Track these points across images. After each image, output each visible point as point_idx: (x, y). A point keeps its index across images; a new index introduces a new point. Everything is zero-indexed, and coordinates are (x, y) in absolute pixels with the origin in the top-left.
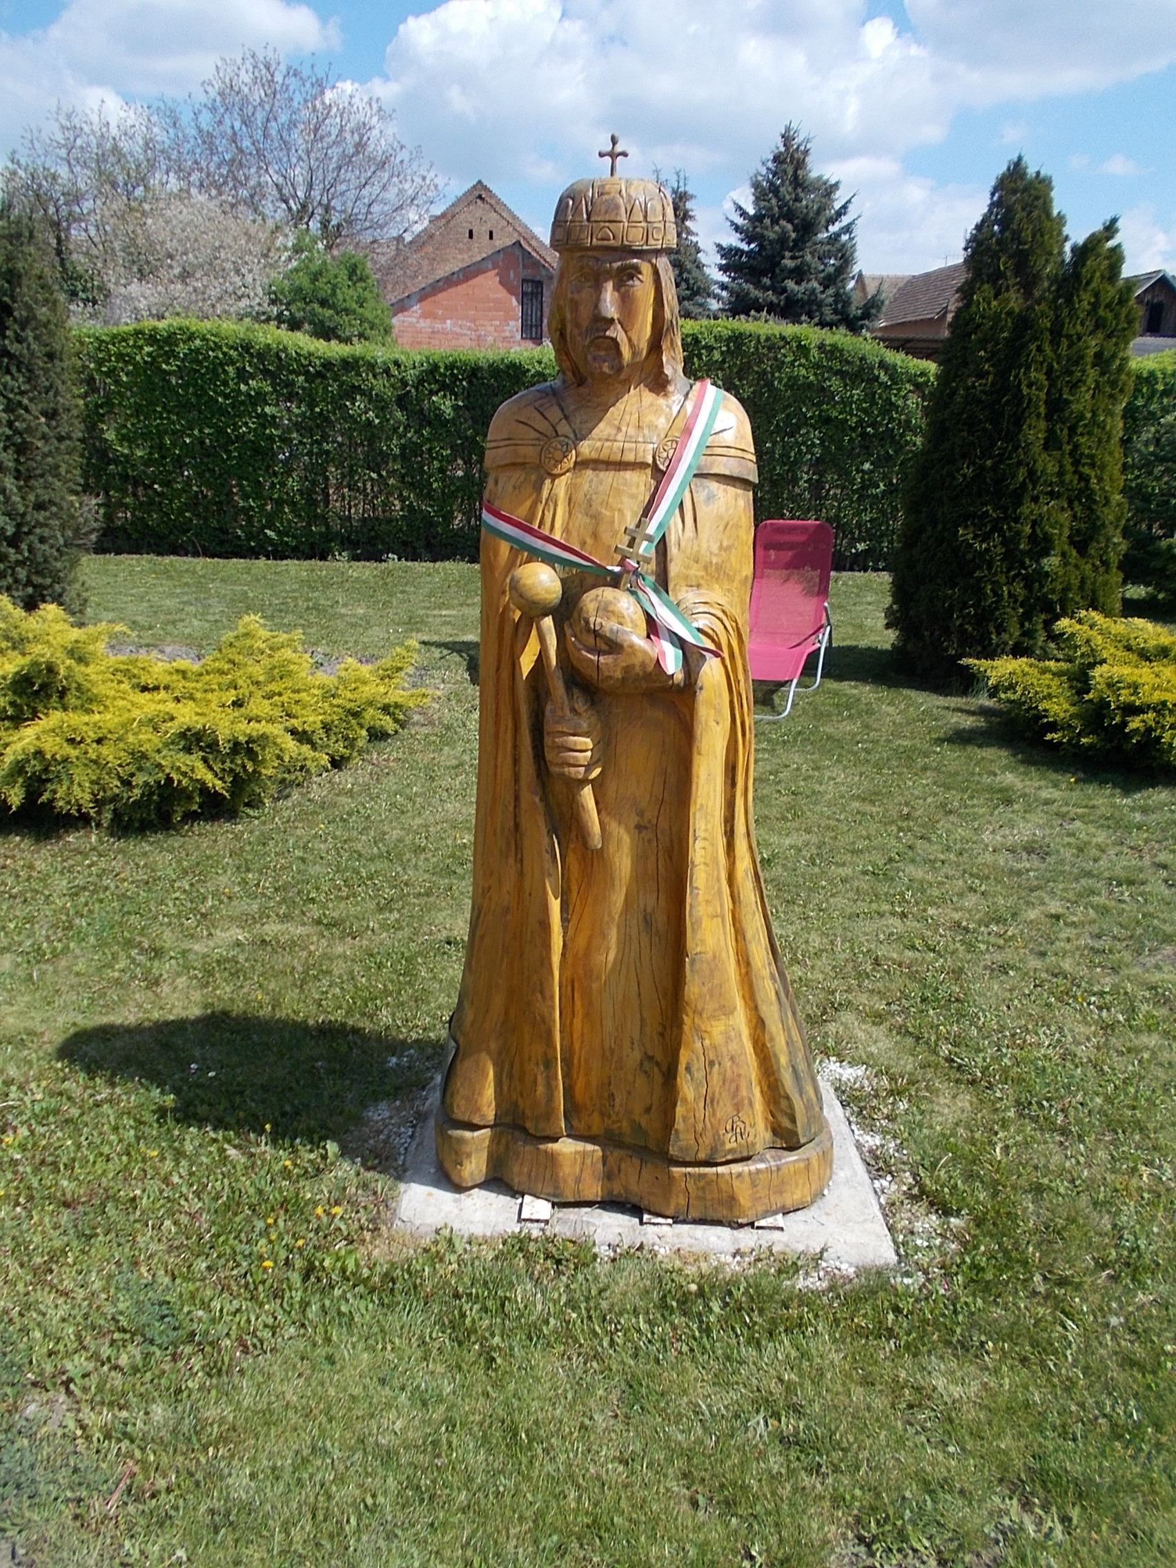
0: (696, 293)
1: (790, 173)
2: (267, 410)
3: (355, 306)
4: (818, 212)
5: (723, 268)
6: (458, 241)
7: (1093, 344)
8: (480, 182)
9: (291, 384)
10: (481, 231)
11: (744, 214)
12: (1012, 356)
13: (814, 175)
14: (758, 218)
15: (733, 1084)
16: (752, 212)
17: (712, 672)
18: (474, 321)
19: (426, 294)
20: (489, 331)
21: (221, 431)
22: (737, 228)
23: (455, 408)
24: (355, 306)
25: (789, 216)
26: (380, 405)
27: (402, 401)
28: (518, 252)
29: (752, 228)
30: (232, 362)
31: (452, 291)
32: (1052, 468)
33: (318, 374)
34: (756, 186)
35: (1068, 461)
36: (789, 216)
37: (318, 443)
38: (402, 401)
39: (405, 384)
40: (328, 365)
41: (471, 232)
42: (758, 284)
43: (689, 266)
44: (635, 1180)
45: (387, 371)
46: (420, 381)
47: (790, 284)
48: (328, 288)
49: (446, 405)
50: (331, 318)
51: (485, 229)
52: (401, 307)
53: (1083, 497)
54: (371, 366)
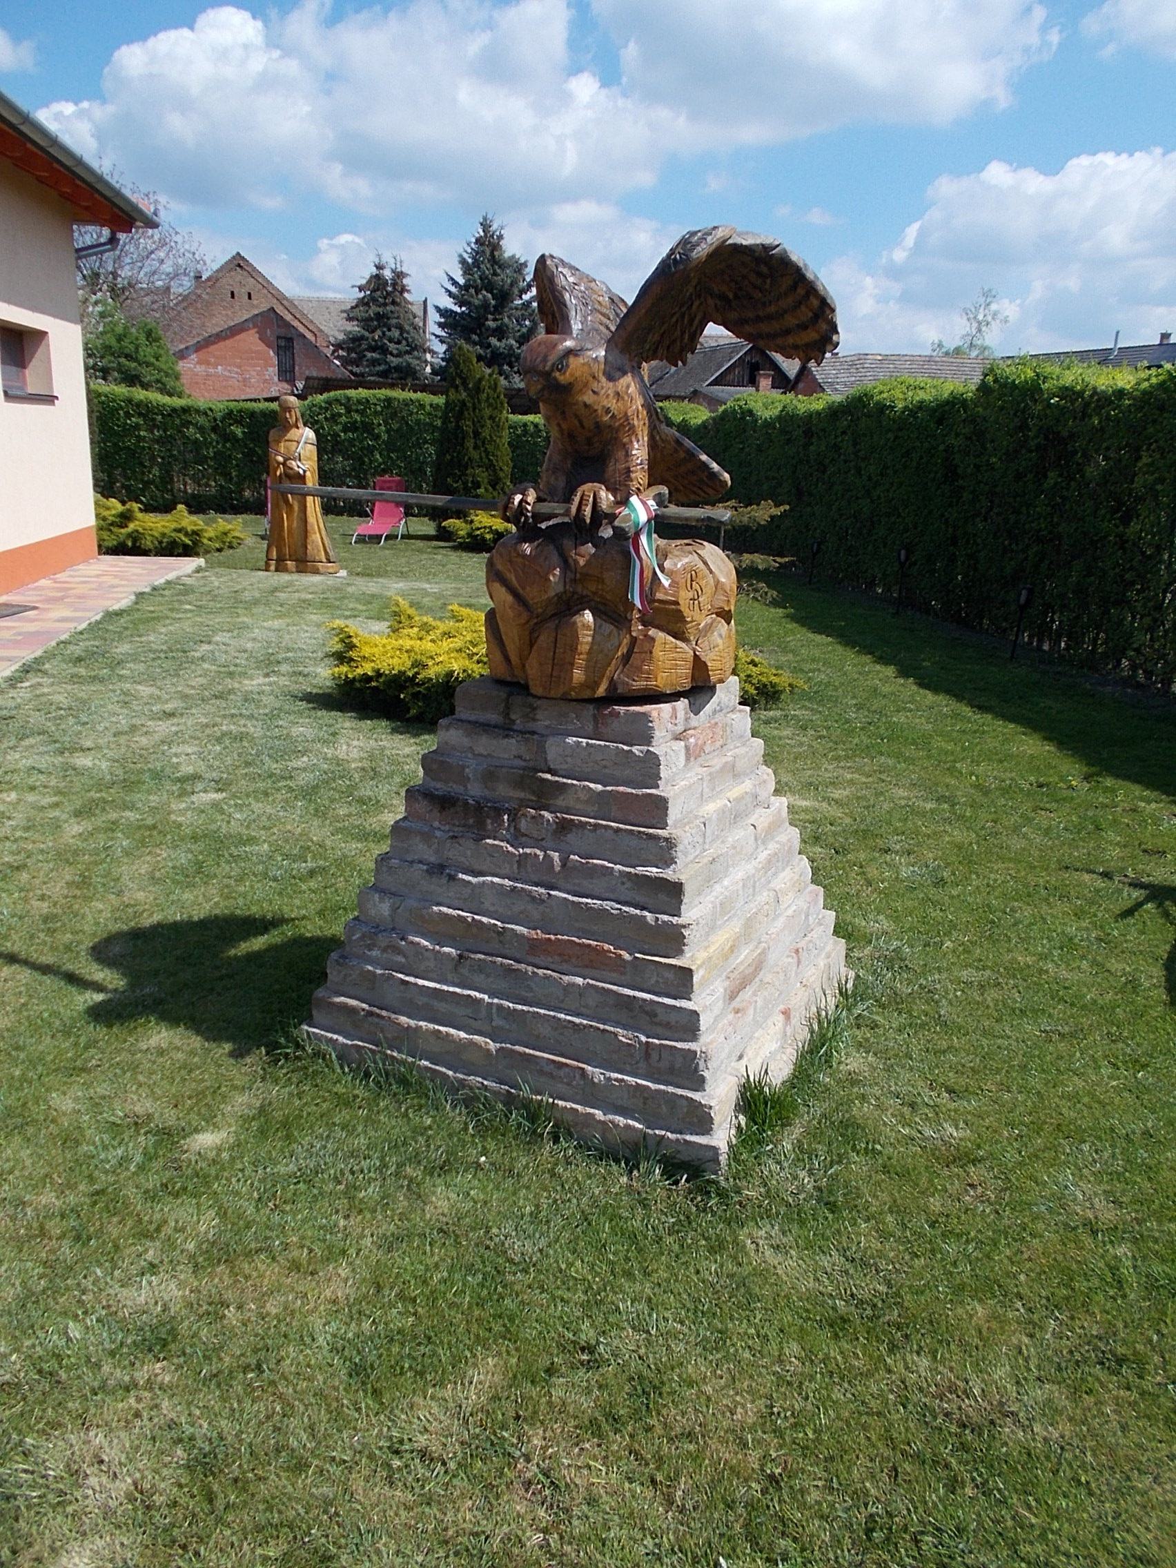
0: (415, 348)
1: (488, 254)
2: (142, 433)
3: (152, 360)
4: (512, 285)
5: (440, 325)
6: (222, 300)
7: (487, 412)
8: (238, 254)
9: (154, 420)
10: (241, 292)
11: (455, 283)
12: (460, 416)
13: (506, 255)
14: (466, 287)
15: (317, 546)
16: (461, 281)
17: (308, 474)
18: (239, 367)
19: (199, 347)
20: (253, 374)
21: (115, 445)
22: (450, 294)
23: (244, 433)
24: (152, 360)
25: (489, 287)
26: (201, 429)
27: (215, 429)
28: (272, 315)
29: (462, 294)
30: (122, 408)
31: (222, 344)
32: (477, 457)
33: (169, 415)
34: (463, 262)
35: (483, 455)
36: (489, 287)
37: (169, 450)
38: (215, 429)
39: (215, 420)
40: (174, 410)
41: (232, 293)
42: (468, 340)
43: (407, 328)
44: (301, 567)
45: (206, 413)
46: (223, 419)
47: (494, 341)
48: (132, 347)
49: (239, 431)
50: (135, 369)
51: (244, 291)
52: (182, 355)
53: (490, 466)
54: (198, 411)
